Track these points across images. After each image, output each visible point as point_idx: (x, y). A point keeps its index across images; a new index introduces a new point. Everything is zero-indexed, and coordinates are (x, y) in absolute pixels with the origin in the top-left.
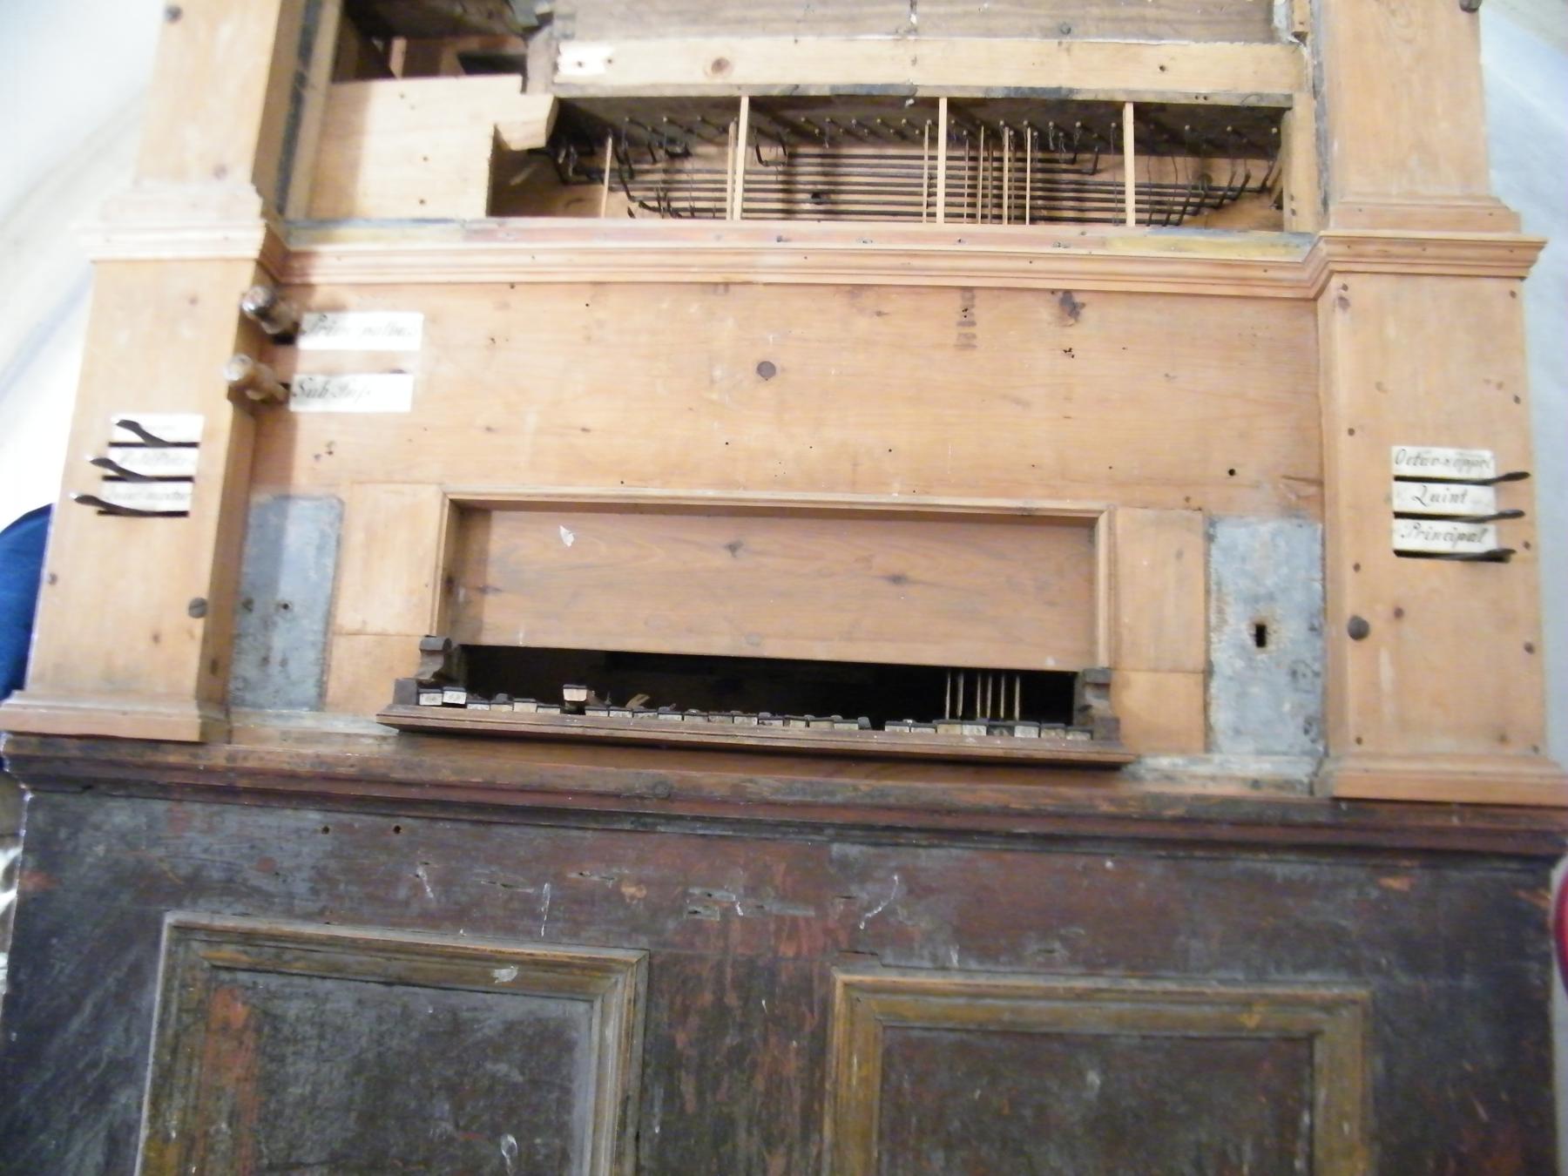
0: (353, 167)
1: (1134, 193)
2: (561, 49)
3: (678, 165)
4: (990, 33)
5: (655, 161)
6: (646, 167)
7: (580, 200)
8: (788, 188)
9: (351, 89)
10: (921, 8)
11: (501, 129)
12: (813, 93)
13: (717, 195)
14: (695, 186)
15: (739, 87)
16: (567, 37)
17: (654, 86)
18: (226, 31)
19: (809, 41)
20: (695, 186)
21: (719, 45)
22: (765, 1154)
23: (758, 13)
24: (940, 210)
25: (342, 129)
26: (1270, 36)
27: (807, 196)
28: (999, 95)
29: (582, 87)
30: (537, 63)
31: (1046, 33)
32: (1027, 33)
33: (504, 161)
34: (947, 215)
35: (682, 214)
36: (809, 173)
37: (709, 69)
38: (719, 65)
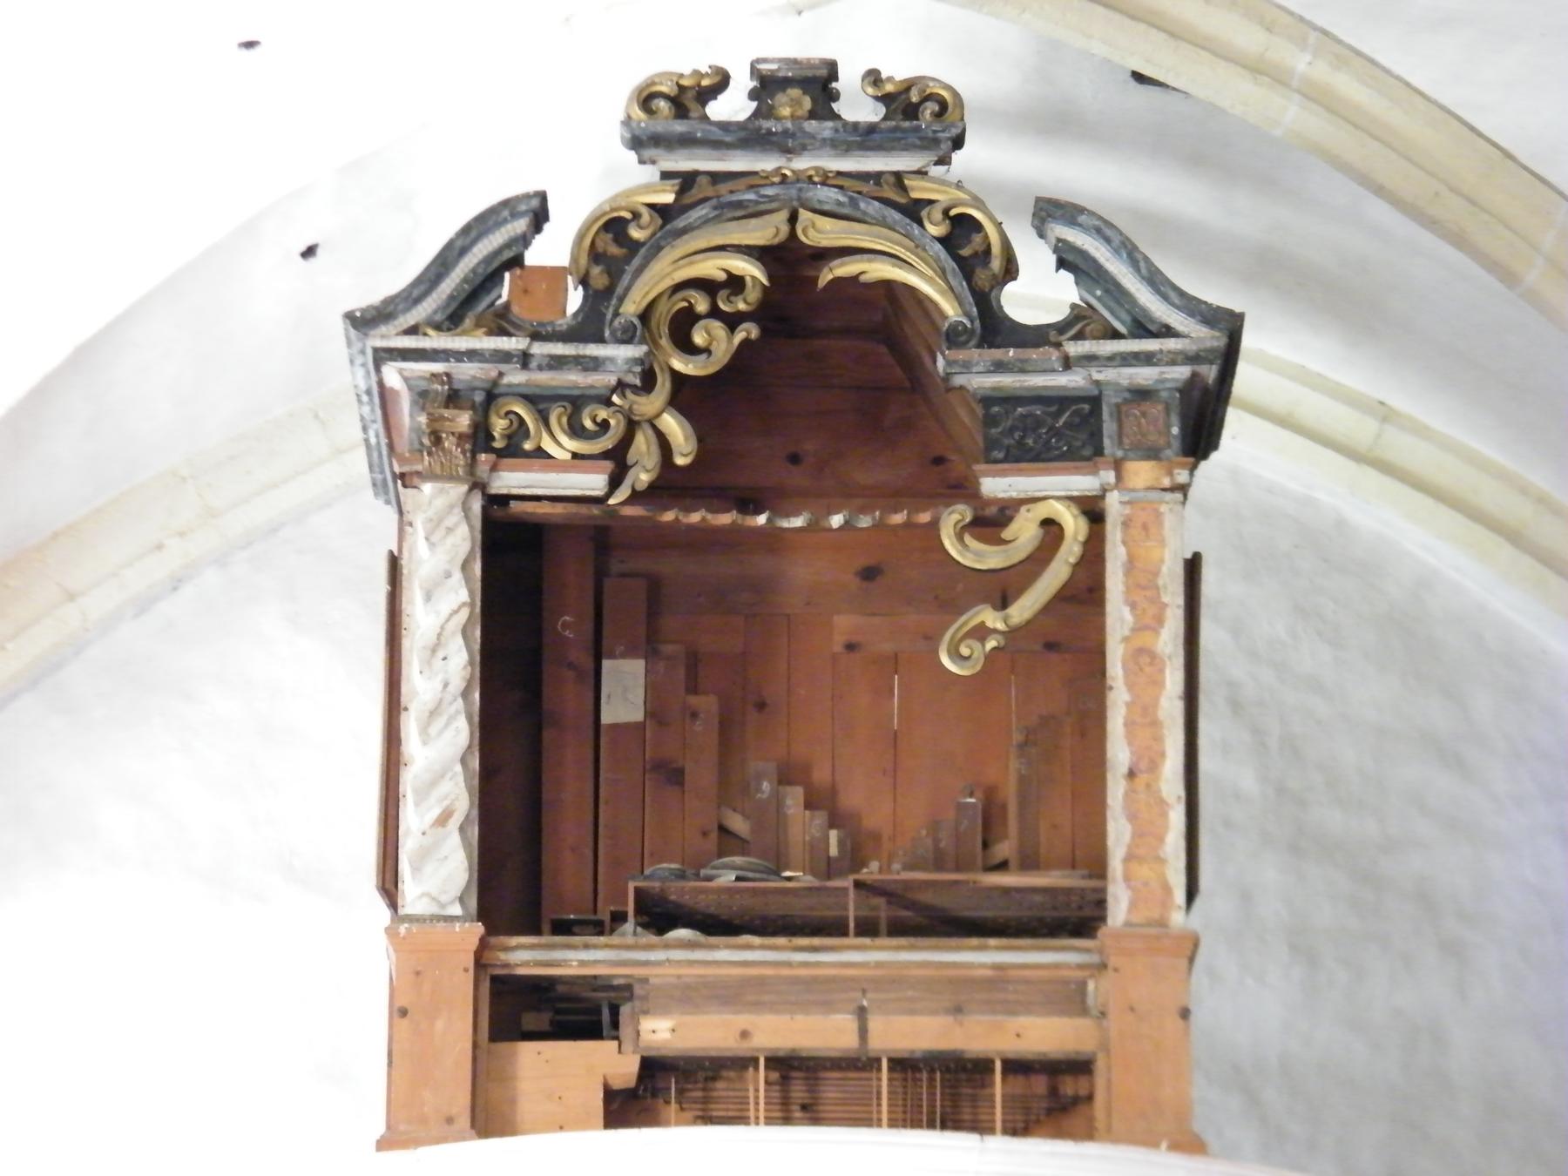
0: (513, 1102)
1: (757, 1127)
2: (641, 1021)
3: (710, 1085)
4: (912, 1012)
5: (696, 1082)
6: (690, 1086)
7: (646, 1110)
8: (785, 1103)
9: (503, 1047)
10: (869, 995)
11: (608, 1078)
12: (804, 1054)
13: (739, 1107)
14: (731, 1100)
15: (758, 1050)
16: (646, 1012)
17: (704, 1049)
18: (440, 1024)
19: (800, 1018)
20: (731, 1100)
21: (743, 1020)
22: (655, 351)
23: (766, 998)
24: (762, 1115)
25: (506, 1077)
26: (1084, 1011)
27: (798, 1108)
28: (918, 1055)
29: (658, 1049)
30: (625, 1031)
31: (948, 1012)
32: (934, 1012)
33: (610, 1095)
34: (766, 1118)
35: (729, 249)
36: (798, 1092)
37: (738, 1039)
38: (745, 1034)
